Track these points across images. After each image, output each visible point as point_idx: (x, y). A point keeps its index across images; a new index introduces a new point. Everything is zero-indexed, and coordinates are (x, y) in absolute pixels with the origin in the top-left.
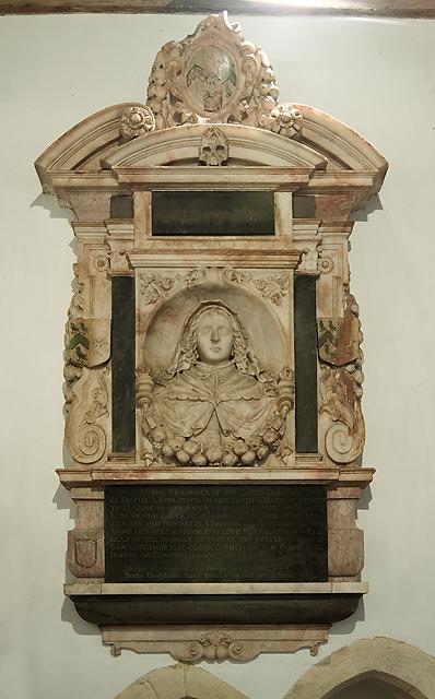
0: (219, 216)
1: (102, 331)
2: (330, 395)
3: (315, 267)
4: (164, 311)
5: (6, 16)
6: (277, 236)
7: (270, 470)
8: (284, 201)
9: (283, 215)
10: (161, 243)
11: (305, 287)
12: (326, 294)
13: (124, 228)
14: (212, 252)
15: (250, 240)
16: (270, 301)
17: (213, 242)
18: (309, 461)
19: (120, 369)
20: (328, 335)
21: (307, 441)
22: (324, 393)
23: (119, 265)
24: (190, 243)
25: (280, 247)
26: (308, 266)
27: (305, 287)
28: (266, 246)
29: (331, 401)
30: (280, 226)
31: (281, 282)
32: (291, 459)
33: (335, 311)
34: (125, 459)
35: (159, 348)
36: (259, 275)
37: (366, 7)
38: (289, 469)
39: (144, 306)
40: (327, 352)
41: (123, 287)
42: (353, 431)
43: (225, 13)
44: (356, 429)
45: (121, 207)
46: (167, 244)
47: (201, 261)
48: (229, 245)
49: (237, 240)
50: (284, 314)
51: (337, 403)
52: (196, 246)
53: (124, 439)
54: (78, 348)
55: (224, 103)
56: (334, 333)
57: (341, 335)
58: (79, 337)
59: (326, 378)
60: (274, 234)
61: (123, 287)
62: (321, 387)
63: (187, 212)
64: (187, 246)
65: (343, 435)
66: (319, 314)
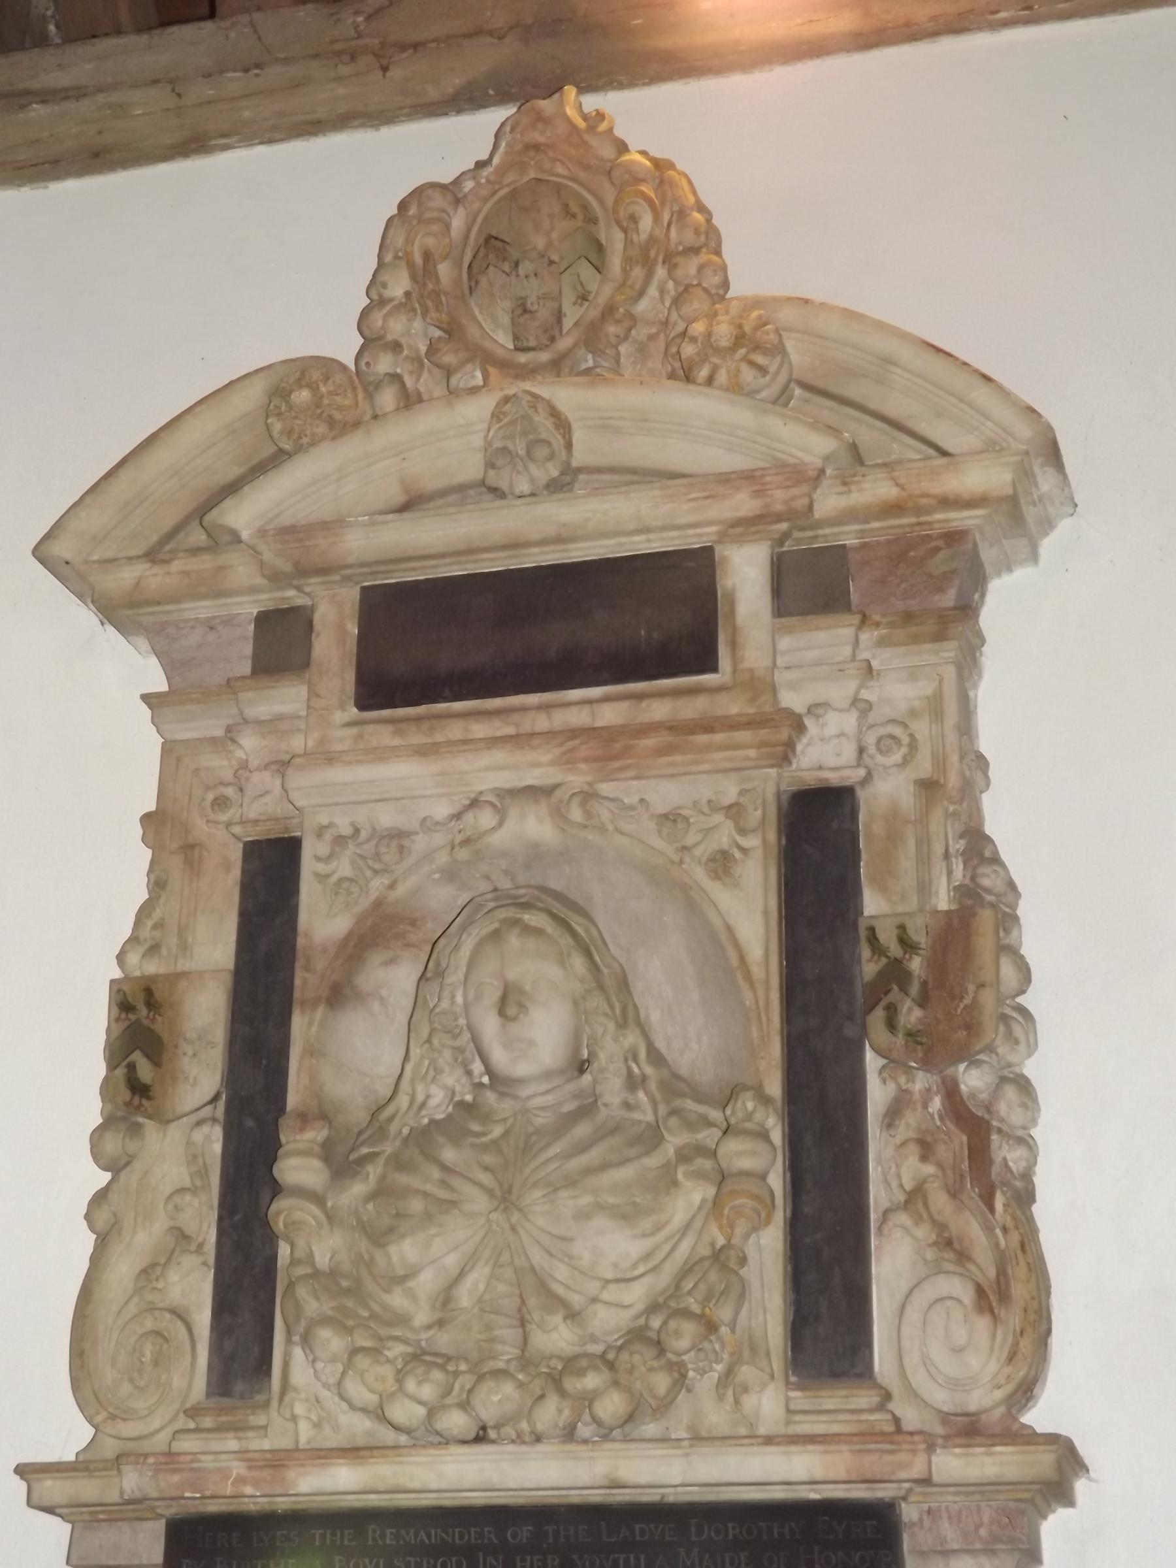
0: (554, 636)
1: (205, 1011)
2: (912, 1169)
3: (849, 751)
4: (378, 931)
5: (23, 189)
6: (724, 674)
7: (698, 1438)
8: (746, 574)
9: (743, 610)
10: (381, 729)
11: (818, 835)
12: (893, 838)
13: (286, 698)
14: (518, 740)
15: (640, 697)
16: (700, 875)
17: (535, 710)
18: (841, 1404)
19: (250, 1123)
20: (895, 973)
21: (829, 1325)
22: (889, 1167)
23: (262, 807)
24: (463, 720)
25: (734, 706)
26: (824, 755)
27: (818, 835)
28: (691, 709)
29: (915, 1197)
30: (734, 645)
31: (734, 811)
32: (769, 1402)
33: (924, 888)
34: (237, 1428)
35: (353, 1053)
36: (666, 793)
37: (844, 22)
38: (755, 1445)
39: (322, 919)
40: (891, 1025)
41: (272, 870)
42: (990, 1299)
43: (570, 91)
44: (1013, 1294)
45: (281, 643)
46: (399, 733)
47: (489, 771)
48: (578, 718)
49: (607, 699)
50: (750, 911)
51: (939, 1200)
52: (480, 730)
53: (243, 1352)
54: (132, 1067)
55: (568, 323)
56: (916, 964)
57: (938, 965)
58: (140, 1028)
59: (893, 1114)
60: (714, 669)
61: (272, 870)
62: (879, 1146)
63: (448, 643)
64: (455, 730)
65: (958, 1313)
66: (872, 904)
